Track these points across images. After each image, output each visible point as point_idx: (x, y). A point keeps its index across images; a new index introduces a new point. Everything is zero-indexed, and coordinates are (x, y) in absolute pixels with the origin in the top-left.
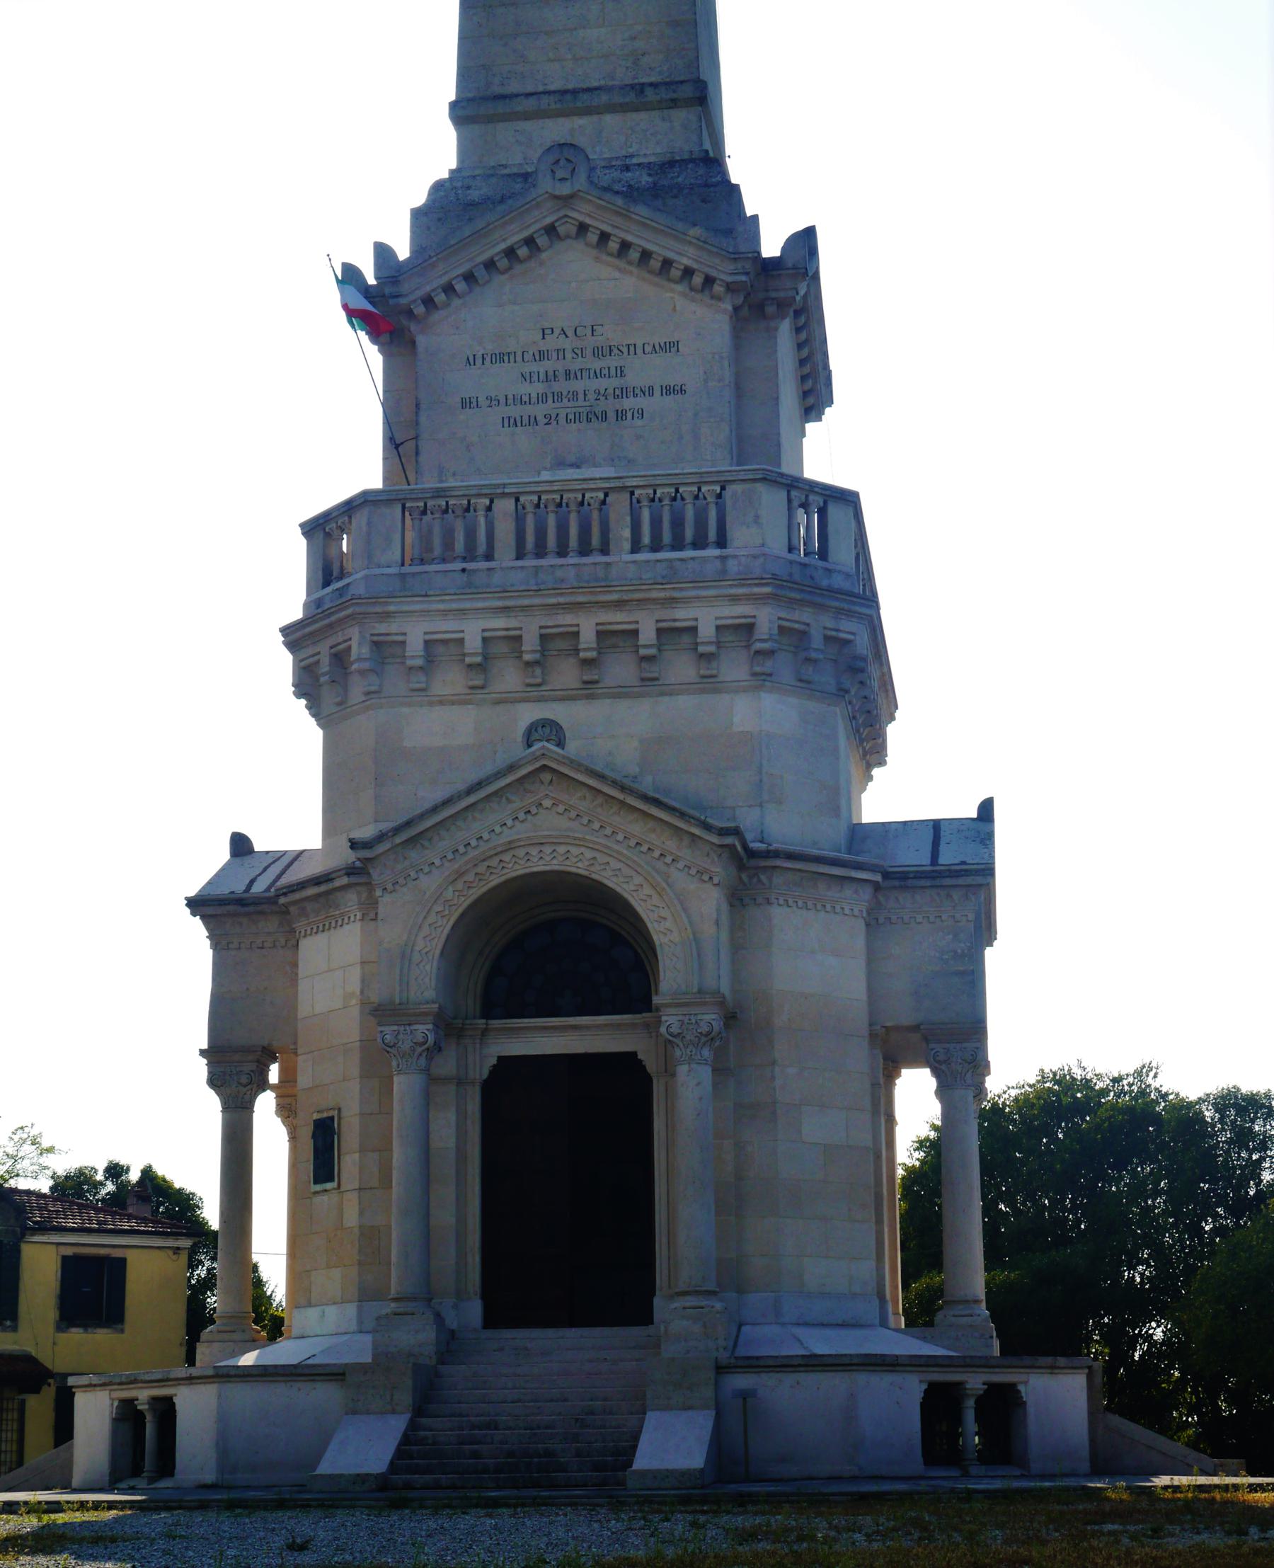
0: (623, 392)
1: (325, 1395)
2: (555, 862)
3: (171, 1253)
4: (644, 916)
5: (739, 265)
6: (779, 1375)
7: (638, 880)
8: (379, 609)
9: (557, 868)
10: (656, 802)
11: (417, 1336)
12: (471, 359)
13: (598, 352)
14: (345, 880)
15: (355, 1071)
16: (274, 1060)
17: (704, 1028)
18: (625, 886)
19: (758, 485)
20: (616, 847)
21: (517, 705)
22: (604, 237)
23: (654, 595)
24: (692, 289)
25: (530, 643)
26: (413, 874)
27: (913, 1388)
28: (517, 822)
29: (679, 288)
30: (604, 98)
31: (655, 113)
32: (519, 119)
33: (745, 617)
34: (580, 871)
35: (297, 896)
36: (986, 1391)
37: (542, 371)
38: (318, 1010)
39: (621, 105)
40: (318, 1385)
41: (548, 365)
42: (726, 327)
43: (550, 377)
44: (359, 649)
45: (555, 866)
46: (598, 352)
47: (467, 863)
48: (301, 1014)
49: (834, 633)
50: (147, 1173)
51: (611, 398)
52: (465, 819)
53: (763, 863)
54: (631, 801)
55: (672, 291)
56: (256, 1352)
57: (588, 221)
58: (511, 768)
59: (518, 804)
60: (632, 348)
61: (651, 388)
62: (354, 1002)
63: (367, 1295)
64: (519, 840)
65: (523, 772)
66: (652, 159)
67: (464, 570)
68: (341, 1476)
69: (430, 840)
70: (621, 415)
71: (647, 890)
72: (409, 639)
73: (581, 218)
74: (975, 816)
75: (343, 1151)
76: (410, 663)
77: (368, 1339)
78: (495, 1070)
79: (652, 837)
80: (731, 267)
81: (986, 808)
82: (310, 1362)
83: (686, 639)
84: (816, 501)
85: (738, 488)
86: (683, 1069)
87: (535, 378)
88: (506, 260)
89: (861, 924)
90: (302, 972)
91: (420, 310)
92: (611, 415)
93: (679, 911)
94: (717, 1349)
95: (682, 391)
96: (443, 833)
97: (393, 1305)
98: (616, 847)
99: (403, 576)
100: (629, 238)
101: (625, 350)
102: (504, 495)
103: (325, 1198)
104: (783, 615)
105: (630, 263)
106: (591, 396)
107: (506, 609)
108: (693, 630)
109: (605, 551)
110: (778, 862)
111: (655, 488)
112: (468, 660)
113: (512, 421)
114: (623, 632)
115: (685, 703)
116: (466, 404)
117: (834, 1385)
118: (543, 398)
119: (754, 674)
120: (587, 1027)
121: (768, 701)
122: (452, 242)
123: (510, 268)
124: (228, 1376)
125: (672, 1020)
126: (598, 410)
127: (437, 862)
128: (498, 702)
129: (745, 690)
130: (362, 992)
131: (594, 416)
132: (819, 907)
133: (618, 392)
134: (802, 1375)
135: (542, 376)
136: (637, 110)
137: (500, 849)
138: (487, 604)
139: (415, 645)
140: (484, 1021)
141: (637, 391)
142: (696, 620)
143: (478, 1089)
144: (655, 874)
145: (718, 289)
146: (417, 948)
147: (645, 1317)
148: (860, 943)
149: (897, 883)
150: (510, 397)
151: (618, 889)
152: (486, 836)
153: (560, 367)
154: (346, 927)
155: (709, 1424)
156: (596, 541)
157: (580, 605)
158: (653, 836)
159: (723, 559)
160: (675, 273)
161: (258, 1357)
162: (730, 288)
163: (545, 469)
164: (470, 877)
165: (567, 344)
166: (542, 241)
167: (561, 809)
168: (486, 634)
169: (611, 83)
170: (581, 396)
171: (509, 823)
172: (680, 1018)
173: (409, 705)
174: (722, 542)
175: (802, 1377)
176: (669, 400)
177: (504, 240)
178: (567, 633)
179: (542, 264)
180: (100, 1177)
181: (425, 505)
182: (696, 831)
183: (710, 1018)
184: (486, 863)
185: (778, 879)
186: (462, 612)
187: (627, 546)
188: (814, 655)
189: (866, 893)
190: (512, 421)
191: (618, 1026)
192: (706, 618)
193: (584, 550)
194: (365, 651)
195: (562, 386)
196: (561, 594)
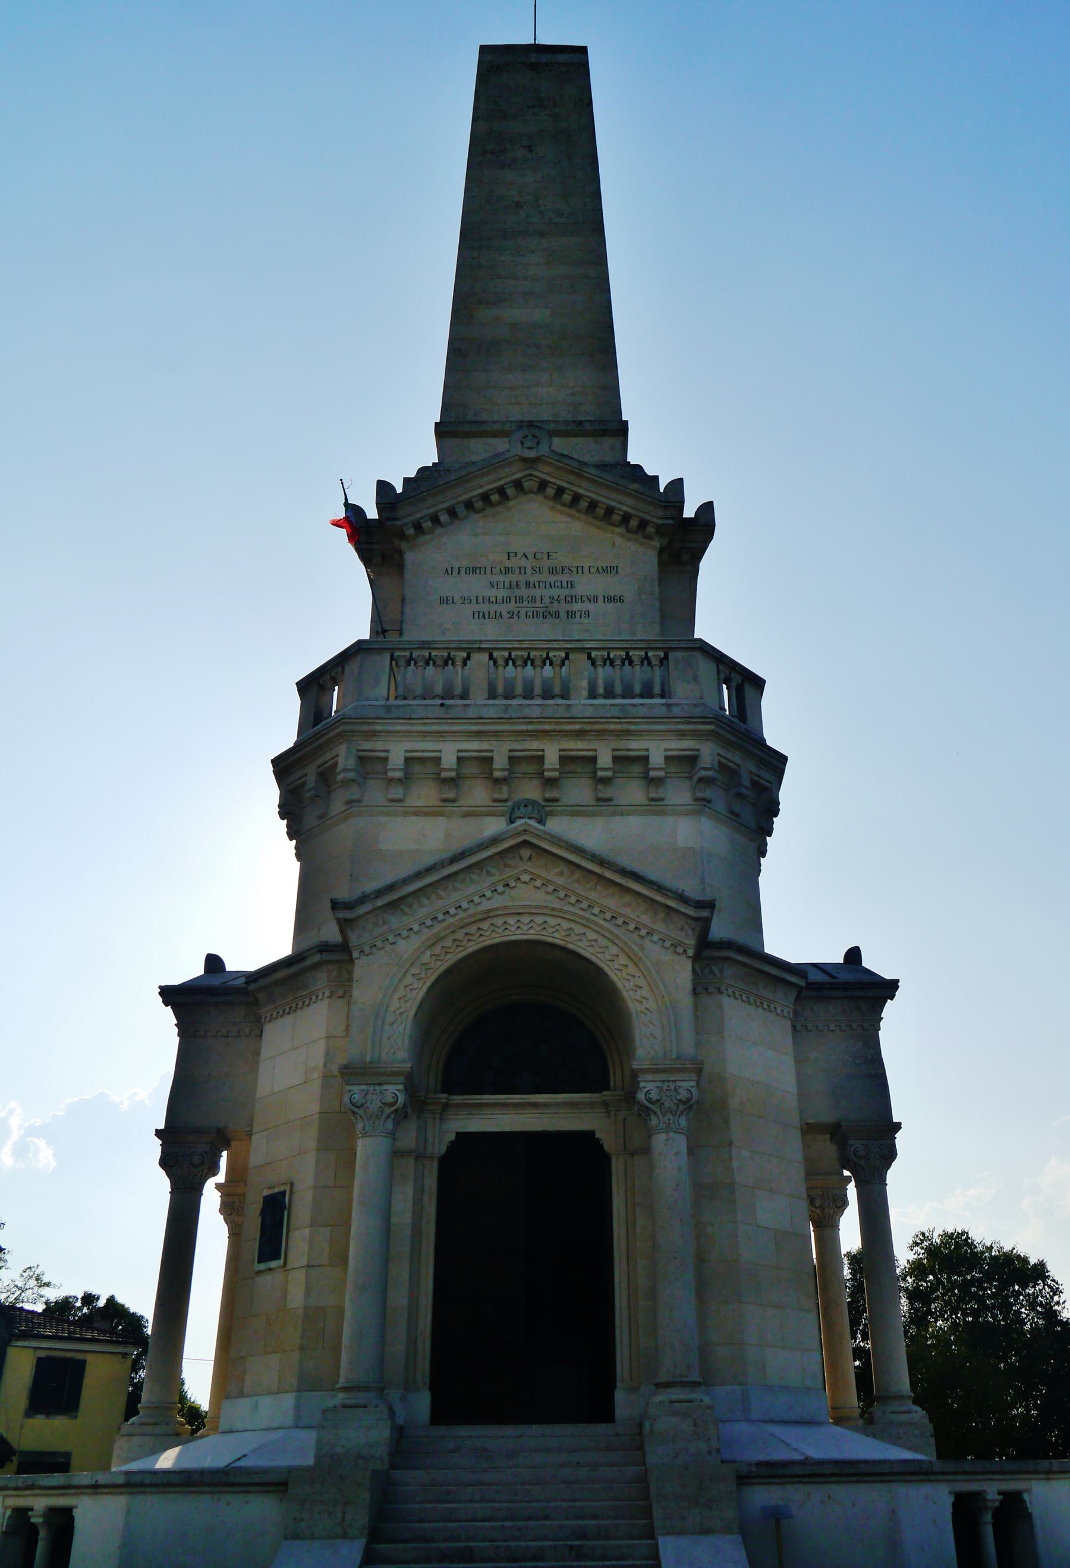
0: (573, 599)
1: (259, 1511)
2: (532, 931)
3: (120, 1357)
4: (619, 984)
7: (614, 950)
8: (365, 728)
9: (534, 937)
10: (635, 876)
11: (367, 1434)
13: (553, 571)
14: (317, 958)
15: (312, 1144)
16: (227, 1146)
17: (683, 1095)
18: (600, 956)
20: (593, 918)
22: (560, 491)
23: (612, 727)
24: (628, 531)
25: (500, 762)
26: (391, 938)
29: (618, 530)
31: (591, 439)
34: (556, 941)
36: (1002, 1502)
38: (276, 1089)
40: (253, 1498)
43: (513, 586)
45: (532, 935)
46: (553, 571)
47: (445, 929)
48: (259, 1095)
50: (111, 1300)
52: (445, 888)
53: (717, 954)
54: (608, 874)
55: (613, 532)
56: (177, 1449)
59: (497, 877)
60: (580, 569)
62: (316, 1075)
63: (306, 1384)
65: (506, 845)
67: (442, 705)
69: (410, 906)
70: (570, 615)
71: (623, 960)
73: (542, 476)
75: (292, 1226)
76: (391, 774)
77: (311, 1436)
78: (453, 1146)
79: (628, 911)
80: (661, 513)
82: (241, 1463)
83: (637, 769)
84: (736, 679)
85: (679, 655)
90: (263, 1056)
91: (410, 531)
92: (563, 615)
93: (651, 985)
94: (710, 1453)
97: (341, 1395)
100: (580, 491)
101: (574, 570)
102: (480, 650)
104: (722, 752)
105: (579, 511)
106: (547, 601)
108: (645, 759)
111: (609, 649)
116: (443, 601)
117: (869, 1498)
118: (507, 600)
119: (696, 799)
120: (546, 1105)
121: (706, 824)
123: (483, 510)
124: (142, 1485)
125: (650, 1086)
127: (416, 927)
128: (466, 815)
129: (687, 814)
130: (325, 1065)
133: (569, 599)
134: (834, 1487)
135: (507, 584)
137: (479, 917)
140: (445, 1096)
142: (647, 750)
143: (435, 1164)
145: (650, 530)
146: (392, 1009)
147: (598, 1407)
153: (522, 579)
154: (313, 1006)
160: (616, 518)
161: (180, 1456)
162: (660, 530)
164: (448, 943)
165: (528, 564)
167: (538, 883)
170: (538, 599)
171: (488, 894)
172: (659, 1084)
173: (386, 814)
177: (481, 487)
179: (509, 509)
180: (78, 1304)
182: (671, 903)
184: (465, 931)
185: (729, 971)
186: (441, 734)
187: (585, 693)
189: (793, 995)
191: (575, 1105)
192: (657, 751)
194: (351, 763)
195: (523, 592)
196: (530, 723)
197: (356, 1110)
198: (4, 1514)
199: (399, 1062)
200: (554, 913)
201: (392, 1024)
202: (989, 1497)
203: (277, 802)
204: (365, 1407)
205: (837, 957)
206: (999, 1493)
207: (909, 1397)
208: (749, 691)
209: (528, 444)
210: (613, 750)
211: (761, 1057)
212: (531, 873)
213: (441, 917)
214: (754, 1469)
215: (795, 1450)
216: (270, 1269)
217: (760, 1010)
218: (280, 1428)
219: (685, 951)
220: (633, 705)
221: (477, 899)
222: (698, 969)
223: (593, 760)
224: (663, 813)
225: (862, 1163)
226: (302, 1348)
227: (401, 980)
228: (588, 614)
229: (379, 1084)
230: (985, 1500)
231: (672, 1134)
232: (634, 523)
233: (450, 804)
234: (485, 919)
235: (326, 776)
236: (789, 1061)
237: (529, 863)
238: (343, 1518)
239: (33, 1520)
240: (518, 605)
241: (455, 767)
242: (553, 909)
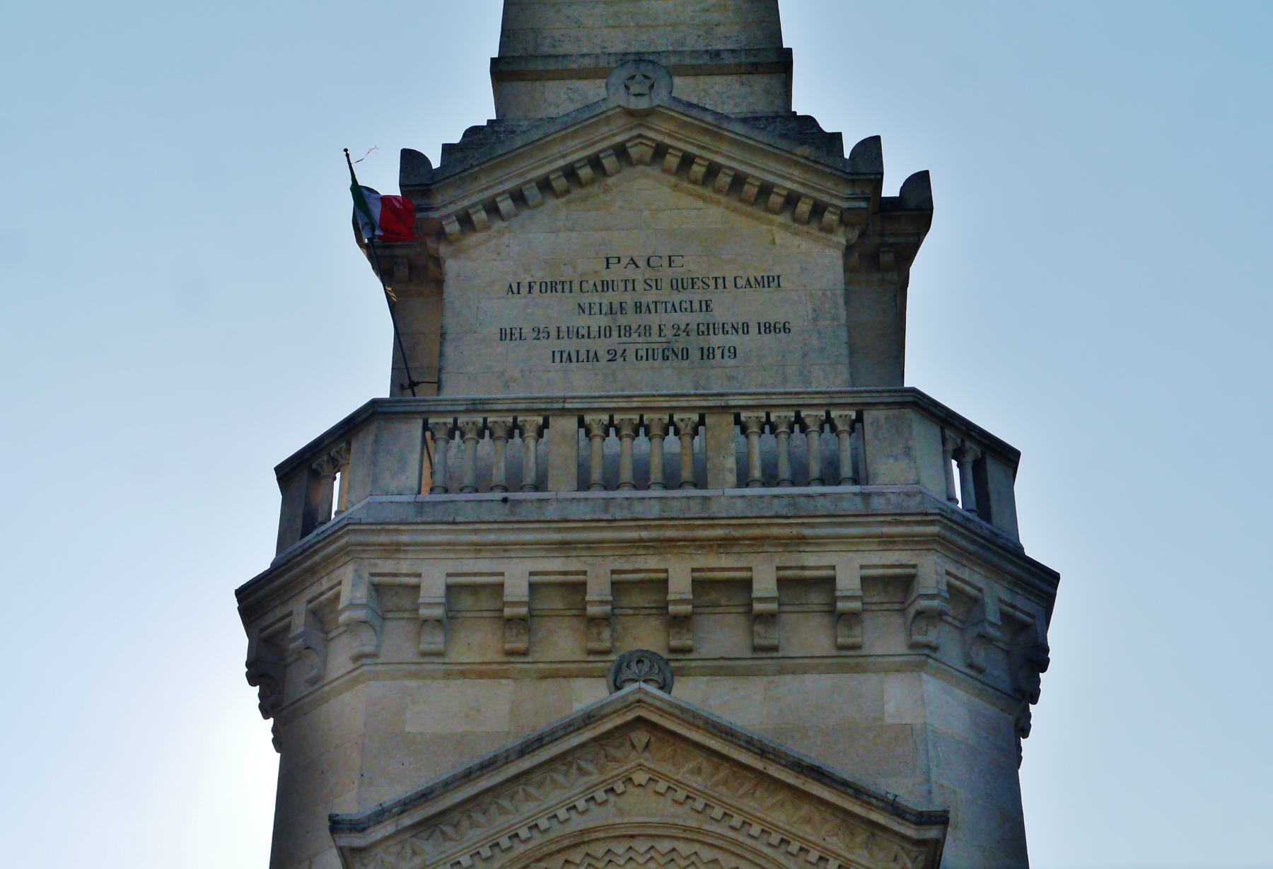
0: (710, 328)
5: (858, 190)
8: (384, 538)
12: (515, 287)
13: (677, 285)
21: (571, 680)
22: (687, 161)
23: (775, 531)
24: (795, 220)
25: (598, 590)
29: (780, 219)
31: (734, 77)
32: (572, 78)
33: (901, 566)
37: (605, 303)
39: (693, 67)
42: (839, 264)
46: (677, 285)
51: (693, 335)
52: (512, 798)
55: (771, 223)
59: (595, 778)
60: (720, 282)
64: (595, 829)
67: (505, 500)
69: (456, 826)
70: (706, 353)
73: (659, 138)
76: (424, 612)
79: (806, 831)
80: (846, 191)
83: (817, 598)
87: (596, 309)
88: (564, 181)
91: (453, 227)
92: (695, 354)
95: (786, 329)
96: (478, 816)
99: (420, 506)
100: (719, 159)
101: (712, 283)
102: (564, 412)
104: (952, 570)
105: (718, 191)
106: (668, 332)
108: (830, 582)
113: (565, 356)
115: (815, 685)
118: (606, 332)
121: (932, 686)
122: (500, 152)
123: (568, 192)
126: (678, 347)
128: (545, 676)
129: (898, 670)
136: (711, 74)
137: (566, 843)
141: (728, 328)
142: (833, 568)
145: (830, 217)
150: (564, 328)
158: (808, 828)
160: (775, 200)
162: (845, 219)
165: (638, 275)
166: (609, 162)
167: (662, 786)
170: (655, 330)
173: (415, 676)
176: (768, 338)
177: (563, 156)
178: (651, 581)
181: (455, 420)
182: (876, 817)
186: (504, 547)
187: (732, 478)
190: (565, 356)
194: (362, 595)
195: (631, 319)
196: (645, 528)
208: (994, 470)
209: (635, 89)
210: (778, 568)
220: (808, 496)
221: (562, 814)
223: (747, 584)
224: (862, 669)
232: (804, 208)
233: (518, 659)
234: (576, 846)
237: (646, 754)
240: (624, 339)
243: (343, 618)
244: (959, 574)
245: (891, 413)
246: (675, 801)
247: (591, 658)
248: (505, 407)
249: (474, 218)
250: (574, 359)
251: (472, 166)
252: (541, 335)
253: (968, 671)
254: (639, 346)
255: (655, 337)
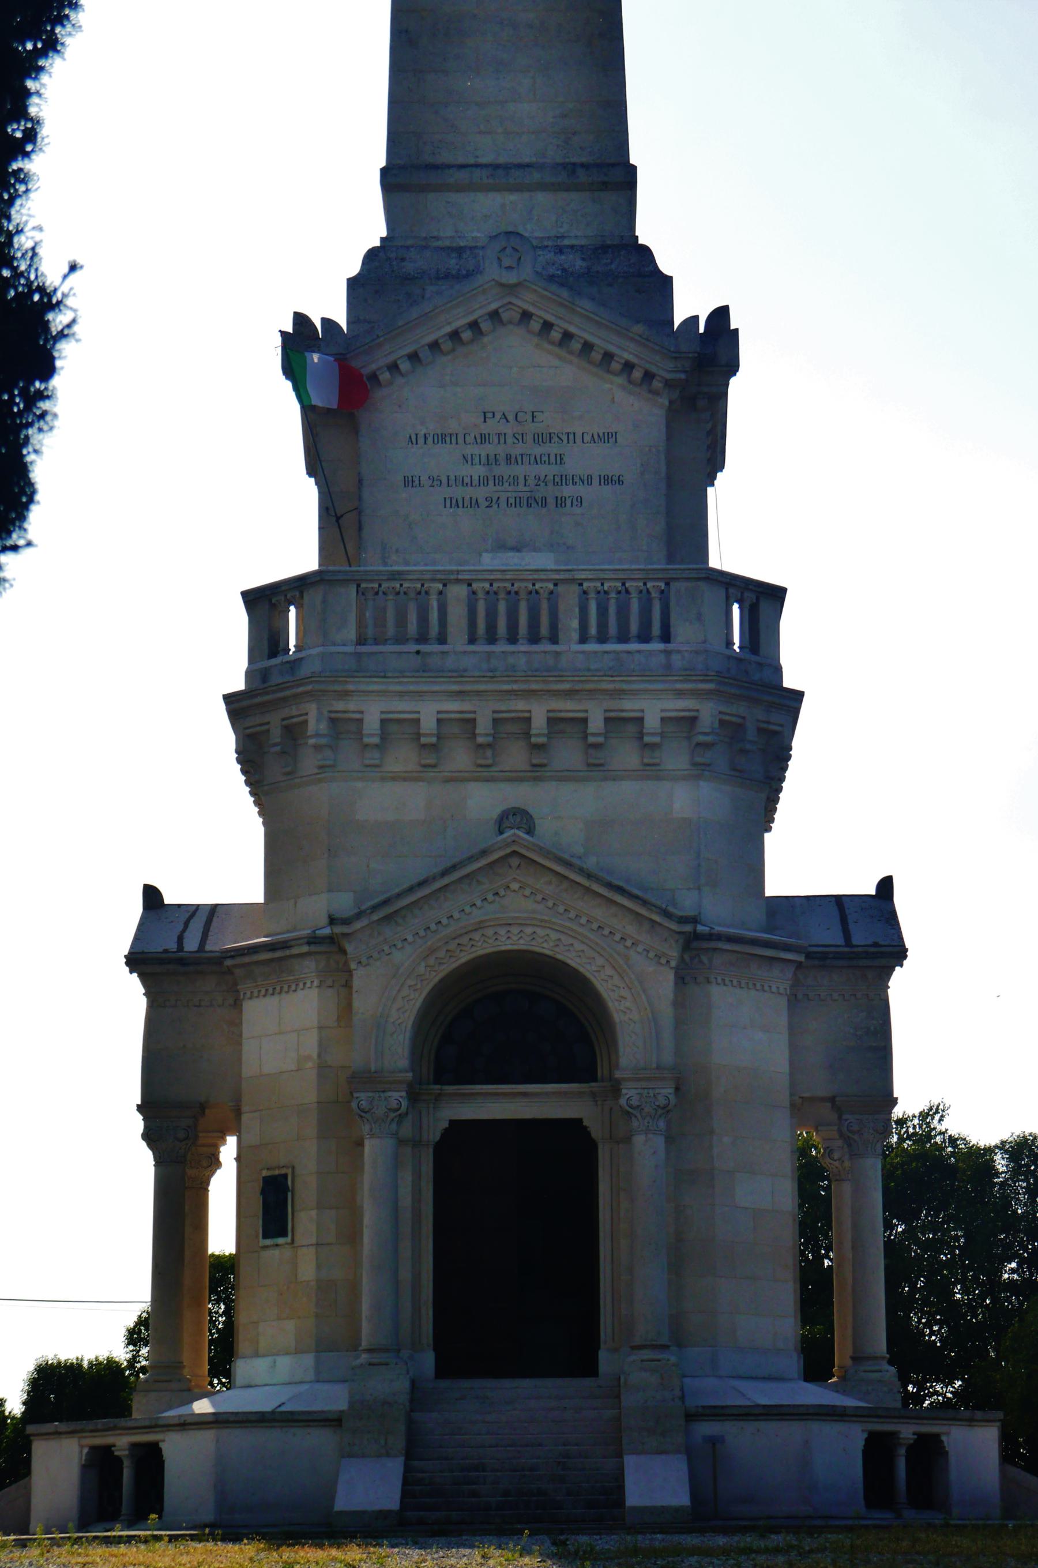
0: (562, 480)
2: (522, 942)
4: (605, 994)
6: (742, 1423)
7: (600, 961)
8: (337, 688)
10: (620, 890)
11: (391, 1384)
13: (539, 439)
14: (305, 949)
17: (661, 1101)
18: (588, 967)
19: (700, 583)
20: (580, 930)
22: (547, 326)
23: (604, 686)
24: (630, 382)
25: (484, 726)
26: (386, 948)
27: (856, 1436)
28: (485, 903)
30: (536, 176)
33: (689, 710)
35: (247, 959)
36: (915, 1441)
37: (483, 454)
39: (553, 184)
41: (489, 449)
43: (491, 461)
44: (315, 723)
45: (522, 945)
46: (539, 439)
49: (765, 726)
51: (551, 484)
53: (705, 945)
54: (595, 887)
55: (612, 383)
57: (531, 309)
58: (484, 853)
60: (571, 436)
61: (590, 478)
62: (310, 1065)
64: (490, 920)
65: (496, 856)
66: (583, 242)
67: (418, 652)
68: (364, 1512)
70: (560, 502)
71: (609, 971)
72: (367, 718)
73: (526, 306)
74: (873, 893)
76: (366, 740)
78: (446, 1133)
80: (670, 365)
81: (886, 885)
82: (283, 1409)
83: (632, 729)
86: (639, 1140)
87: (476, 460)
88: (450, 343)
89: (783, 1002)
90: (244, 1036)
92: (551, 501)
93: (633, 990)
94: (673, 1400)
95: (620, 481)
98: (580, 930)
99: (358, 655)
100: (572, 329)
101: (565, 438)
102: (458, 581)
103: (276, 1252)
105: (571, 353)
106: (531, 481)
107: (460, 694)
108: (640, 720)
109: (554, 639)
110: (721, 945)
112: (423, 740)
113: (454, 502)
114: (572, 719)
116: (409, 482)
117: (792, 1431)
118: (484, 481)
119: (695, 764)
121: (707, 790)
122: (400, 324)
123: (453, 350)
124: (227, 1422)
125: (632, 1092)
127: (410, 938)
130: (319, 1056)
131: (531, 502)
132: (751, 986)
133: (557, 479)
135: (484, 460)
138: (443, 687)
139: (372, 724)
140: (438, 1087)
141: (577, 479)
142: (643, 711)
143: (431, 1150)
144: (616, 956)
145: (657, 384)
147: (585, 1364)
148: (783, 1020)
149: (816, 962)
150: (452, 478)
151: (581, 970)
152: (456, 915)
153: (501, 450)
154: (300, 993)
155: (684, 1467)
156: (544, 630)
157: (533, 692)
159: (668, 653)
160: (615, 366)
163: (487, 551)
164: (441, 954)
165: (508, 429)
166: (485, 326)
167: (527, 892)
168: (441, 716)
169: (541, 161)
170: (521, 480)
172: (639, 1091)
174: (666, 637)
175: (762, 1425)
176: (607, 490)
177: (449, 323)
178: (519, 718)
182: (656, 917)
183: (666, 1091)
184: (457, 941)
186: (421, 694)
187: (575, 636)
188: (748, 747)
189: (789, 972)
190: (454, 502)
192: (653, 710)
193: (534, 639)
194: (323, 727)
195: (503, 470)
196: (516, 681)
197: (363, 1114)
198: (81, 1452)
199: (400, 1072)
200: (543, 924)
201: (392, 1034)
202: (902, 1436)
203: (234, 747)
204: (387, 1364)
205: (870, 889)
206: (914, 1434)
207: (883, 1358)
208: (765, 607)
210: (606, 711)
211: (751, 1033)
212: (520, 882)
213: (433, 927)
214: (700, 1410)
215: (749, 1399)
216: (277, 1245)
217: (753, 993)
218: (301, 1382)
219: (668, 962)
220: (629, 652)
221: (468, 909)
222: (686, 957)
223: (585, 721)
224: (659, 779)
225: (856, 1137)
226: (317, 1316)
227: (399, 991)
228: (580, 501)
229: (383, 1092)
230: (899, 1438)
231: (651, 1136)
232: (637, 374)
233: (430, 769)
234: (476, 930)
235: (294, 732)
236: (782, 1039)
237: (518, 871)
238: (386, 1443)
239: (116, 1453)
240: (497, 488)
241: (435, 732)
242: (542, 921)
243: (312, 741)
244: (728, 711)
245: (689, 584)
246: (536, 902)
247: (480, 769)
248: (415, 577)
249: (381, 378)
250: (461, 505)
251: (378, 337)
252: (435, 483)
253: (732, 773)
254: (509, 494)
255: (521, 487)
